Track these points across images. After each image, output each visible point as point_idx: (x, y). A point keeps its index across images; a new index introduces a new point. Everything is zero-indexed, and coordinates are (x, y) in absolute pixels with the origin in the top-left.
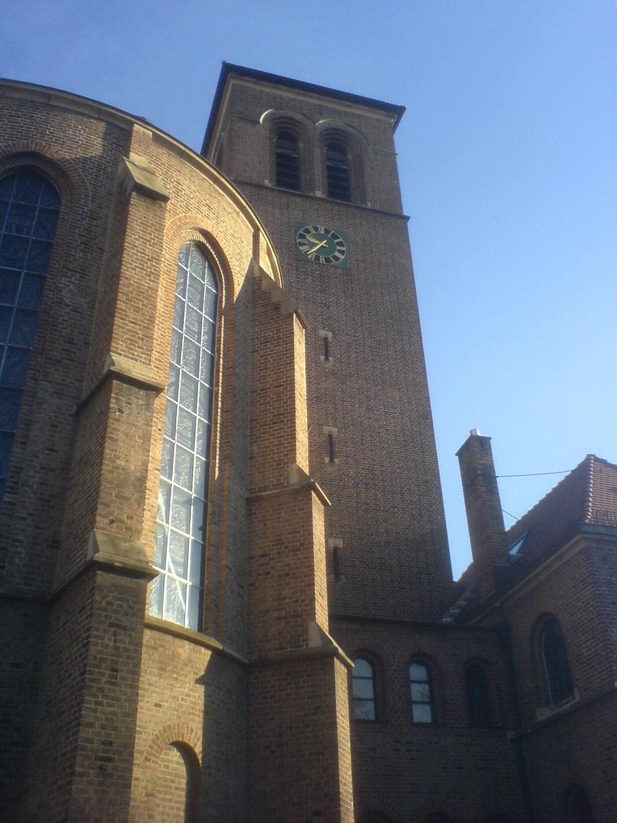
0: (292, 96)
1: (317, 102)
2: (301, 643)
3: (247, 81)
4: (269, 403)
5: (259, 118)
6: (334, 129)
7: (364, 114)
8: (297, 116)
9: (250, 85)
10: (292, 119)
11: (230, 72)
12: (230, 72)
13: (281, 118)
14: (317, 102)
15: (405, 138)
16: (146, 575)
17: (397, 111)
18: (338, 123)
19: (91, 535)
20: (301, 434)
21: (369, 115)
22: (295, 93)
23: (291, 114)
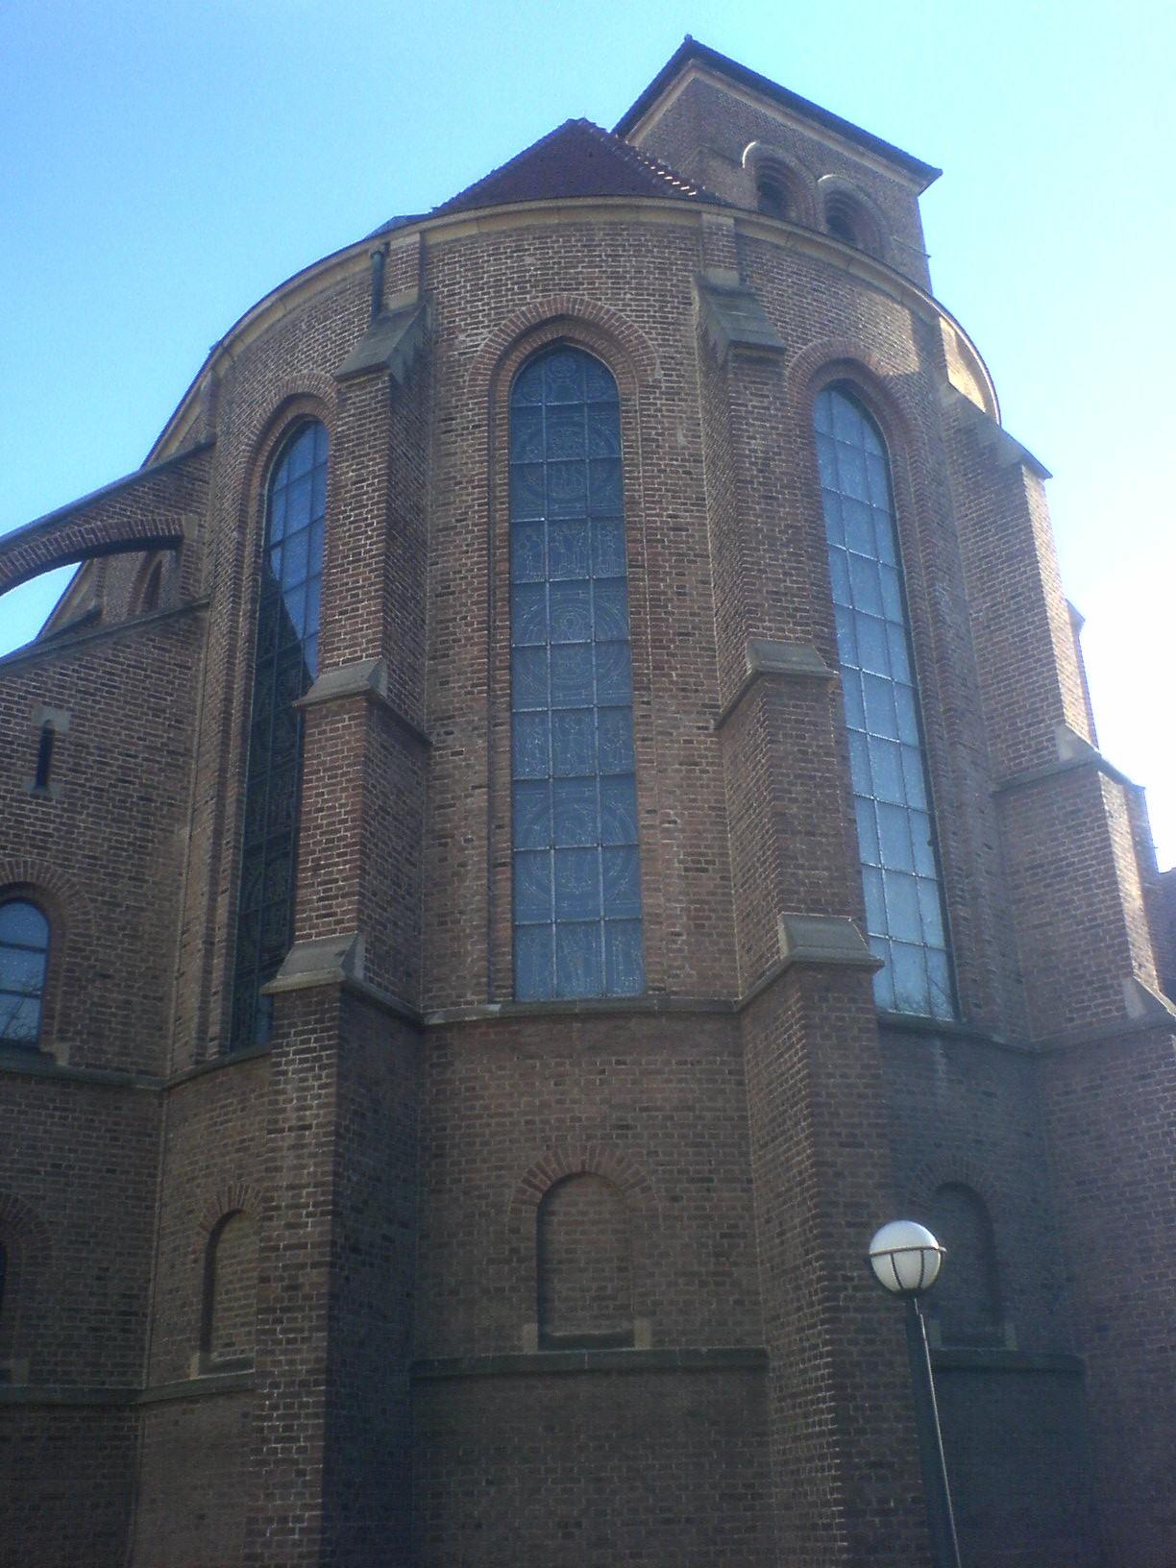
0: (780, 119)
1: (815, 137)
2: (281, 1105)
3: (720, 80)
4: (1082, 976)
5: (740, 154)
6: (840, 193)
7: (881, 170)
8: (793, 162)
9: (719, 86)
10: (781, 163)
11: (692, 54)
12: (692, 54)
13: (767, 159)
14: (815, 137)
15: (931, 203)
16: (871, 967)
17: (924, 174)
18: (847, 183)
19: (1127, 983)
20: (887, 791)
21: (888, 174)
22: (786, 114)
23: (781, 154)
